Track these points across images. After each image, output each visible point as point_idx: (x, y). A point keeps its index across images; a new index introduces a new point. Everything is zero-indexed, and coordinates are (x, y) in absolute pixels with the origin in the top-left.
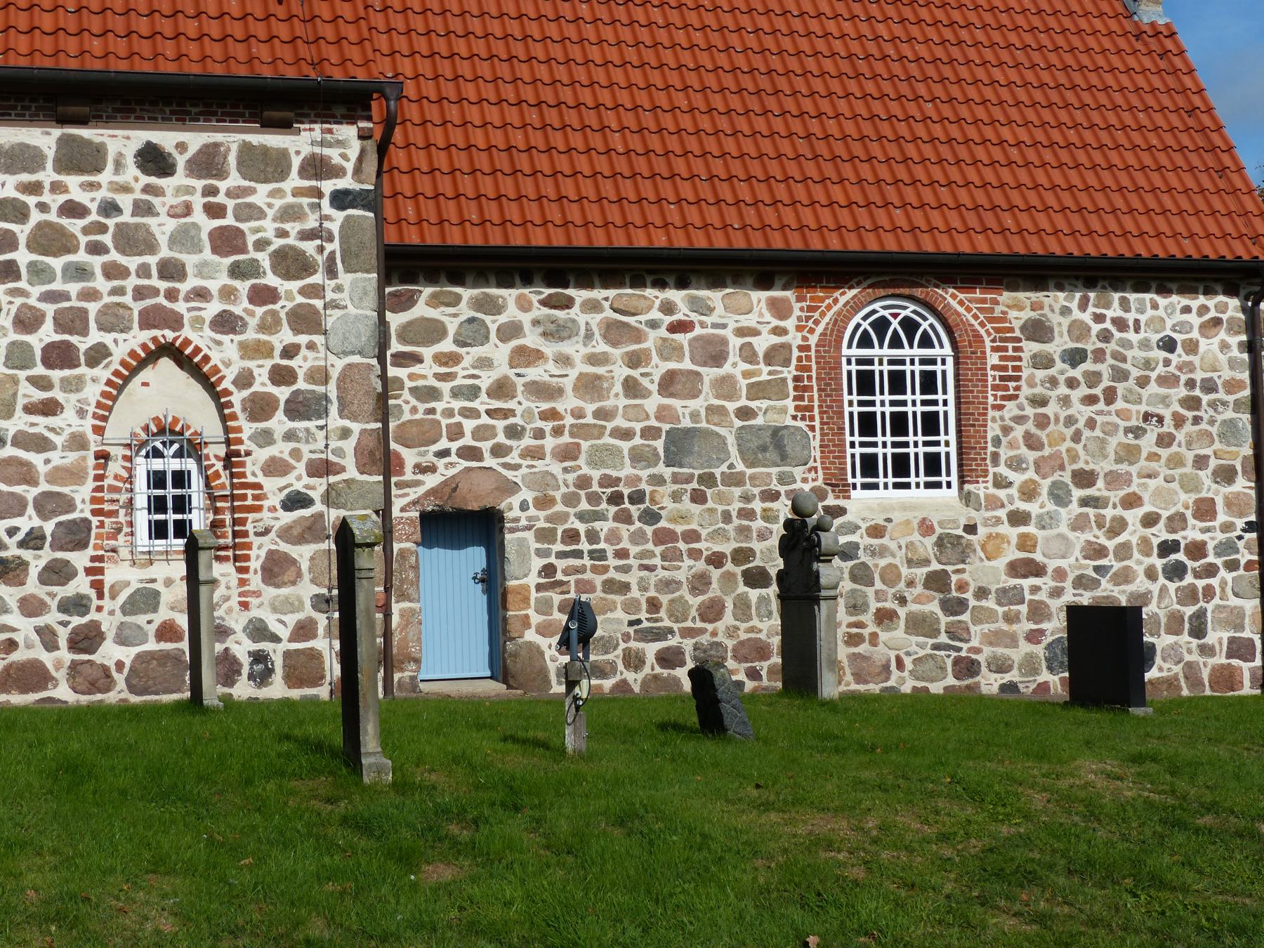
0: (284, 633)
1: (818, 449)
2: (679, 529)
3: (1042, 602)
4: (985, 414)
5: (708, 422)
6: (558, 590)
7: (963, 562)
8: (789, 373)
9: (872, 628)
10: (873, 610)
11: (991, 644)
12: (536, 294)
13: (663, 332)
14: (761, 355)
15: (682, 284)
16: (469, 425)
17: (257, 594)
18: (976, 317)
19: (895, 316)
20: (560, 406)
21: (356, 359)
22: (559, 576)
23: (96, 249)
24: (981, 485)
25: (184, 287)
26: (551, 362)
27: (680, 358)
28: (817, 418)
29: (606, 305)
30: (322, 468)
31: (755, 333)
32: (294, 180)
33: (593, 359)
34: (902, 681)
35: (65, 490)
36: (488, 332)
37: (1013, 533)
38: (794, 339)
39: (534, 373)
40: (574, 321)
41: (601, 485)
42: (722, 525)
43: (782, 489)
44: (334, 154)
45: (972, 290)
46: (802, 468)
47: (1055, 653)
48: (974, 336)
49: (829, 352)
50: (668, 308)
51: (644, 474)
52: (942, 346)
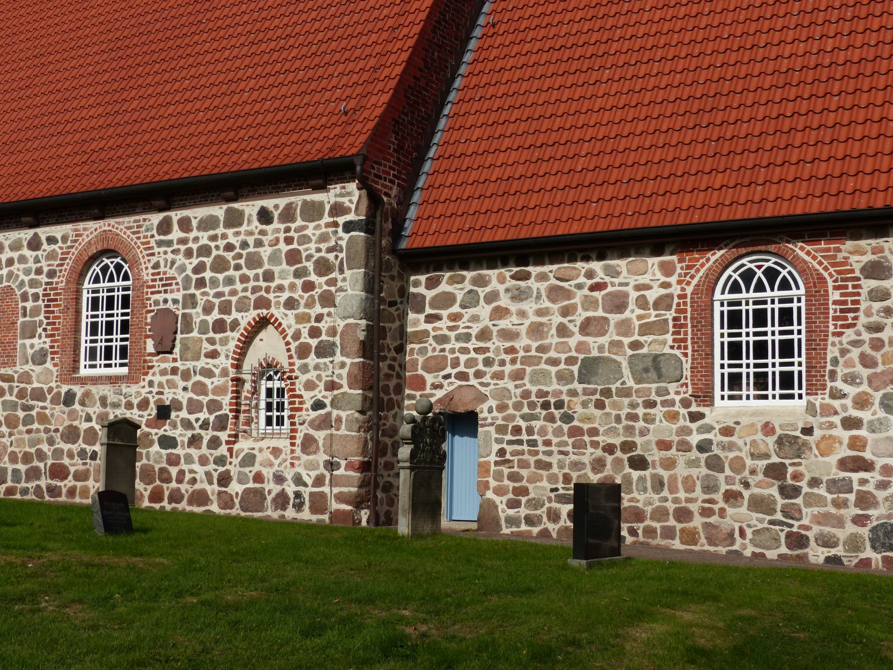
0: (309, 482)
1: (689, 370)
2: (586, 427)
3: (869, 493)
4: (826, 340)
5: (609, 352)
6: (507, 465)
7: (799, 457)
8: (670, 315)
9: (722, 504)
10: (722, 490)
11: (819, 523)
12: (508, 272)
13: (586, 291)
14: (651, 303)
15: (601, 257)
16: (463, 358)
17: (298, 458)
18: (820, 263)
19: (759, 267)
20: (517, 345)
21: (351, 321)
22: (508, 456)
23: (238, 267)
24: (820, 397)
25: (273, 285)
26: (514, 315)
27: (596, 309)
28: (690, 347)
29: (551, 275)
30: (332, 386)
31: (648, 287)
32: (327, 219)
33: (540, 313)
34: (744, 547)
35: (219, 398)
36: (479, 299)
37: (845, 435)
38: (676, 290)
39: (504, 324)
40: (529, 288)
41: (537, 397)
42: (614, 425)
43: (659, 400)
44: (345, 200)
45: (818, 242)
46: (676, 384)
47: (879, 537)
48: (818, 278)
49: (701, 298)
50: (590, 274)
51: (565, 389)
52: (798, 288)
